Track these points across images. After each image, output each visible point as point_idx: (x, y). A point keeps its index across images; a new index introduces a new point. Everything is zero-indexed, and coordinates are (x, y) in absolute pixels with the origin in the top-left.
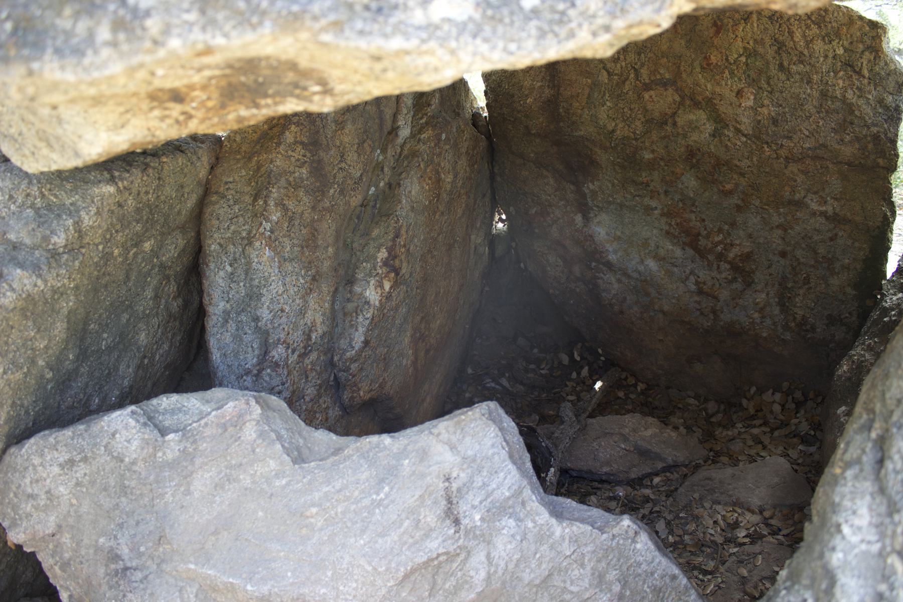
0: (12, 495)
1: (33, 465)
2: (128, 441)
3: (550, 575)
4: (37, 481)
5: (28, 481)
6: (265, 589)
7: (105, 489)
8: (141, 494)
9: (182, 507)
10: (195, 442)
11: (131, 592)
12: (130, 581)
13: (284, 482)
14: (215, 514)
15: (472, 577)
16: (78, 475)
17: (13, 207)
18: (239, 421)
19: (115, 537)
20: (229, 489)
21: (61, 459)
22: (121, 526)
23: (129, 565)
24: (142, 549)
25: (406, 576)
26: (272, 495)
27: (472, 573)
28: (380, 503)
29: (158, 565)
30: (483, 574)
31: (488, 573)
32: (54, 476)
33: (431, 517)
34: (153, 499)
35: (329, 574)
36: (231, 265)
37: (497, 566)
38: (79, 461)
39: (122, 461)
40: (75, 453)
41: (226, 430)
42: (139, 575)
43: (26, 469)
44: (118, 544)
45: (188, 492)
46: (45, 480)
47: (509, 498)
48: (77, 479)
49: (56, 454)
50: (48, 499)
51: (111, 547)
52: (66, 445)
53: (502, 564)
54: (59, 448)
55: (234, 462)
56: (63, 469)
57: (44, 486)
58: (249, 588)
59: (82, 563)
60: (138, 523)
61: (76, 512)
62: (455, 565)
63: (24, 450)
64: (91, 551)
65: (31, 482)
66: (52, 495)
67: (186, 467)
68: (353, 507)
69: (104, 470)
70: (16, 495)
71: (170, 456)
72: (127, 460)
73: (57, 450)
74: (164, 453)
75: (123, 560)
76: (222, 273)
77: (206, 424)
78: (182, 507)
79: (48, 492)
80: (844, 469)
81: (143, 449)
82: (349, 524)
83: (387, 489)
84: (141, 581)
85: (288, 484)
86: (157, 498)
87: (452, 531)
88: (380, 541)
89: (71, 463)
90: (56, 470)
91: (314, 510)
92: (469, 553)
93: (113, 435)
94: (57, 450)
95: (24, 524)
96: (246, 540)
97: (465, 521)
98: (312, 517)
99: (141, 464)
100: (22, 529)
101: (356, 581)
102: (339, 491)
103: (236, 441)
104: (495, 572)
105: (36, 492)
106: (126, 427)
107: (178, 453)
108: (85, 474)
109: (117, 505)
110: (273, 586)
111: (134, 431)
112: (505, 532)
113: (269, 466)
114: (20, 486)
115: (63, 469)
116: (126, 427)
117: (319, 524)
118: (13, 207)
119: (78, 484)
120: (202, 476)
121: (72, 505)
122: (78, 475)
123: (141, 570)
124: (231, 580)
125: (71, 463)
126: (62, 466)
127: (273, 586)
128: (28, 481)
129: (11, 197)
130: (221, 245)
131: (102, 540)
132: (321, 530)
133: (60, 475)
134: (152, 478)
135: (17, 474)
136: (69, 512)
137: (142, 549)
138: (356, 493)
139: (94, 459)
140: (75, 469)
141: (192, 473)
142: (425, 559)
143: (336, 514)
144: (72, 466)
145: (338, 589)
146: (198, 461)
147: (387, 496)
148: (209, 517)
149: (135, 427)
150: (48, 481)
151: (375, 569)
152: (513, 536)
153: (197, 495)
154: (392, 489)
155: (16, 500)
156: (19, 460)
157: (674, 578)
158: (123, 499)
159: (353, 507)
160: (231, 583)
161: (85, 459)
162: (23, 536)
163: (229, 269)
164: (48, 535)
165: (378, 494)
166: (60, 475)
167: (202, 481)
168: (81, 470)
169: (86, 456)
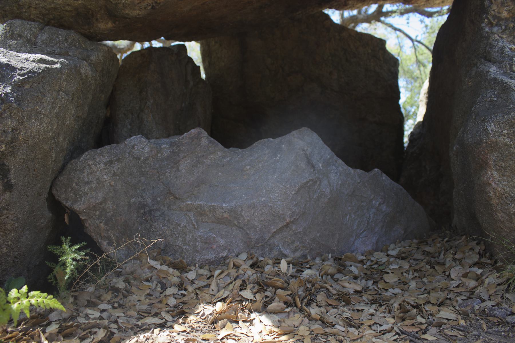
0: (74, 185)
1: (89, 165)
2: (143, 149)
3: (354, 191)
4: (91, 173)
5: (85, 174)
6: (233, 204)
7: (131, 174)
8: (152, 174)
9: (177, 177)
10: (179, 146)
11: (155, 222)
12: (154, 216)
13: (228, 159)
14: (196, 177)
15: (324, 192)
16: (115, 169)
17: (66, 44)
18: (198, 137)
19: (142, 196)
20: (200, 167)
21: (105, 161)
22: (144, 190)
23: (152, 208)
24: (158, 199)
25: (299, 190)
26: (224, 165)
27: (324, 190)
28: (278, 161)
29: (168, 207)
30: (328, 190)
31: (330, 189)
32: (101, 170)
33: (303, 165)
34: (159, 177)
35: (264, 191)
36: (130, 125)
37: (333, 186)
38: (115, 161)
39: (140, 159)
40: (113, 157)
41: (193, 141)
42: (158, 213)
43: (84, 168)
44: (144, 199)
45: (178, 170)
46: (96, 172)
47: (330, 159)
48: (114, 171)
49: (102, 158)
50: (97, 183)
51: (140, 201)
52: (108, 153)
53: (335, 185)
54: (104, 155)
55: (199, 155)
56: (106, 166)
57: (96, 176)
58: (224, 205)
59: (121, 215)
60: (153, 188)
61: (114, 190)
62: (316, 187)
63: (82, 158)
64: (126, 208)
65: (88, 175)
66: (100, 181)
67: (176, 159)
68: (266, 164)
69: (129, 165)
70: (77, 184)
71: (165, 155)
72: (142, 158)
73: (103, 155)
74: (162, 154)
75: (148, 207)
76: (125, 129)
77: (183, 138)
78: (177, 177)
79: (98, 179)
80: (498, 51)
81: (151, 151)
82: (267, 171)
83: (279, 155)
84: (160, 216)
85: (231, 159)
86: (161, 175)
87: (312, 170)
88: (283, 175)
89: (111, 162)
90: (102, 166)
91: (248, 167)
92: (320, 181)
93: (133, 147)
94: (103, 155)
95: (83, 199)
96: (216, 185)
97: (316, 166)
98: (247, 170)
99: (150, 159)
100: (82, 202)
101: (277, 193)
102: (258, 158)
103: (198, 146)
104: (333, 189)
105: (91, 180)
106: (140, 142)
107: (169, 153)
108: (119, 168)
109: (140, 181)
110: (237, 202)
111: (145, 144)
112: (333, 171)
113: (218, 155)
114: (80, 178)
115: (106, 166)
116: (140, 142)
117: (252, 173)
118: (66, 44)
119: (115, 174)
120: (184, 162)
121: (112, 186)
122: (115, 169)
123: (159, 211)
124: (213, 204)
125: (111, 162)
126: (105, 164)
127: (237, 202)
128: (85, 174)
129: (66, 39)
130: (125, 114)
131: (133, 200)
132: (253, 175)
133: (105, 169)
134: (157, 166)
135: (78, 172)
136: (110, 190)
137: (158, 199)
138: (266, 158)
139: (123, 159)
140: (113, 165)
141: (179, 161)
142: (305, 181)
143: (259, 167)
144: (111, 164)
145: (270, 197)
146: (182, 155)
147: (280, 158)
148: (193, 179)
149: (145, 142)
150: (98, 173)
151: (285, 186)
152: (336, 173)
153: (183, 171)
154: (281, 155)
155: (76, 187)
156: (79, 164)
157: (401, 190)
158: (143, 178)
159: (266, 164)
160: (213, 206)
161: (118, 160)
162: (83, 206)
163: (129, 127)
164: (98, 204)
165: (276, 158)
166: (105, 169)
167: (185, 165)
168: (116, 167)
169: (119, 158)
